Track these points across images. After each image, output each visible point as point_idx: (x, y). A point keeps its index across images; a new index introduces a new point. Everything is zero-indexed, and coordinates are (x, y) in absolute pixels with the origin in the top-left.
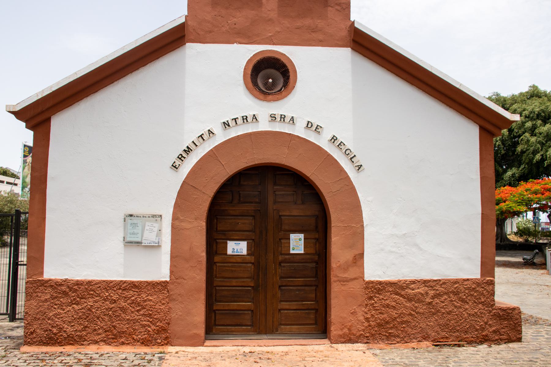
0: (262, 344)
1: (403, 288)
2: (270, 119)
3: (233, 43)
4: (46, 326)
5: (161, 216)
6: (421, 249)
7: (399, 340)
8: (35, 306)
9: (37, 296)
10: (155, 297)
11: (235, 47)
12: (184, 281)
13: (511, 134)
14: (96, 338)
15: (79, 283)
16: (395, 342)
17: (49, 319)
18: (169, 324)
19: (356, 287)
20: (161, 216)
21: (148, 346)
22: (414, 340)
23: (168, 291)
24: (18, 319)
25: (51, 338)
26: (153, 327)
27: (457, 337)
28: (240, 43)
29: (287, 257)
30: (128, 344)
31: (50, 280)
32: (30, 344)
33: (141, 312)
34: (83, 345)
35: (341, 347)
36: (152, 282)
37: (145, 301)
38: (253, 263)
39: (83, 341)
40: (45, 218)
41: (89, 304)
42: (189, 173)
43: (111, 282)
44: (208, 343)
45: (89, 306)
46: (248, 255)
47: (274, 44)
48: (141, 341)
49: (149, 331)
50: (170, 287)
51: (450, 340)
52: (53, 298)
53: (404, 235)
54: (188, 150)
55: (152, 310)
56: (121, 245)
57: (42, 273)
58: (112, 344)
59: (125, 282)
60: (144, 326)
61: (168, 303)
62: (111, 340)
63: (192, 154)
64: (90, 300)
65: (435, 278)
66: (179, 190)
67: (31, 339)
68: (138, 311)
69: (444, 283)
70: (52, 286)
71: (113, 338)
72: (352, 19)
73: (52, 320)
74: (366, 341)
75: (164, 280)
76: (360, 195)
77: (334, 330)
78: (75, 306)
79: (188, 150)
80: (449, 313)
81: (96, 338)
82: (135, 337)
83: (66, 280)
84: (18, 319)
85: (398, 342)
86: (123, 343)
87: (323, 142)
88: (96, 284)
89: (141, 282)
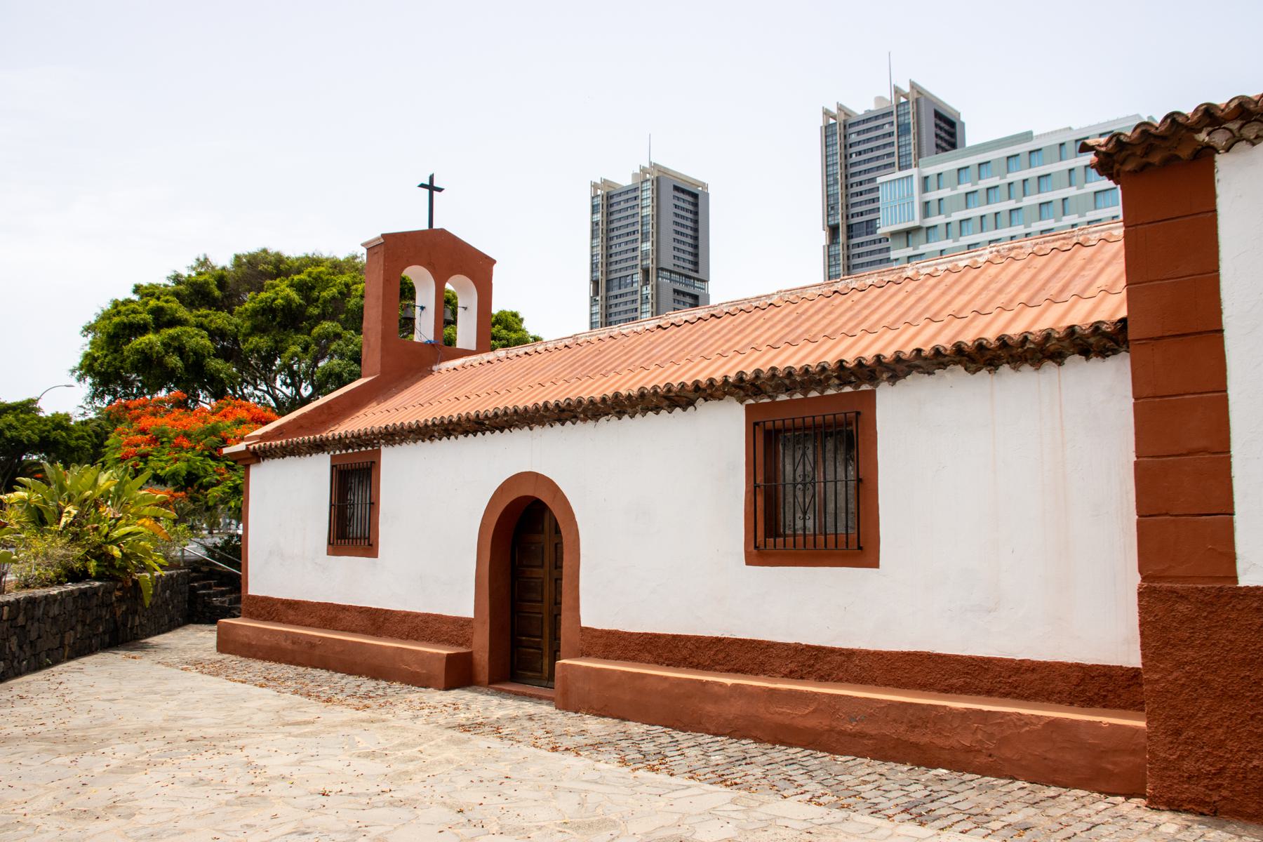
42: (502, 513)
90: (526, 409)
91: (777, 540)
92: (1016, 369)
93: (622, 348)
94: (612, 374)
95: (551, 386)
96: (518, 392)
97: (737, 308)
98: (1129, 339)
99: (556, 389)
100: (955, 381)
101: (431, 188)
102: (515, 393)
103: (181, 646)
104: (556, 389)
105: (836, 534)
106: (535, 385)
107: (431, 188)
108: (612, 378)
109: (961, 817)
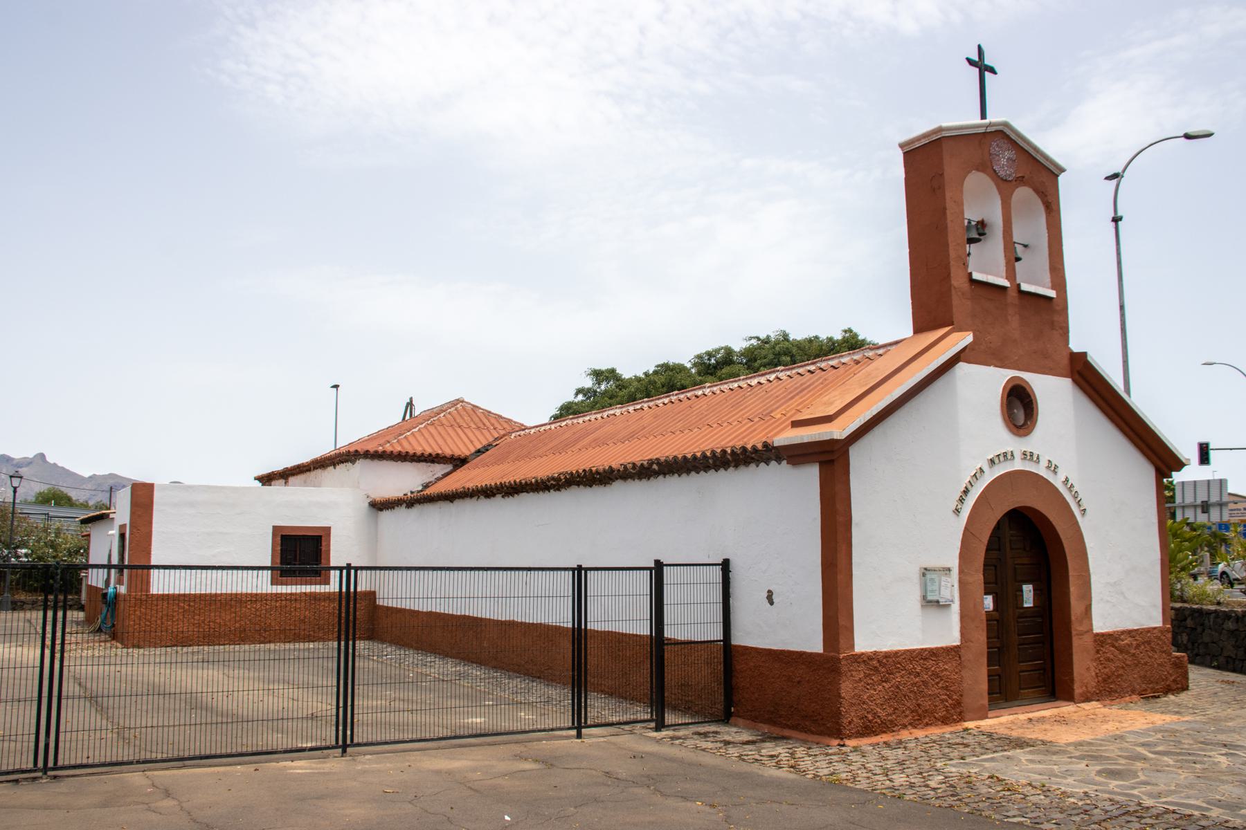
0: (1027, 711)
1: (1116, 640)
2: (1023, 457)
3: (990, 366)
4: (861, 713)
5: (925, 571)
6: (1125, 597)
7: (1117, 695)
8: (851, 688)
9: (852, 675)
10: (950, 665)
11: (992, 370)
12: (972, 644)
13: (753, 458)
14: (905, 721)
15: (887, 655)
16: (1115, 698)
17: (864, 703)
18: (961, 696)
19: (1088, 639)
20: (925, 571)
21: (947, 724)
22: (1127, 695)
23: (960, 657)
24: (668, 726)
25: (866, 727)
26: (950, 701)
27: (1152, 689)
28: (996, 366)
29: (1022, 611)
30: (931, 724)
31: (863, 654)
32: (849, 736)
33: (940, 685)
34: (894, 731)
35: (1082, 705)
36: (947, 647)
37: (942, 671)
38: (997, 620)
39: (894, 727)
40: (852, 575)
41: (897, 680)
42: (968, 517)
43: (914, 651)
44: (991, 714)
45: (897, 683)
46: (994, 610)
47: (1019, 370)
48: (941, 720)
49: (947, 707)
50: (962, 652)
51: (1148, 692)
52: (866, 676)
53: (1115, 583)
54: (966, 492)
55: (948, 682)
56: (918, 605)
57: (852, 646)
58: (918, 727)
59: (925, 650)
60: (943, 701)
61: (960, 671)
62: (917, 722)
63: (969, 495)
64: (898, 675)
65: (1135, 628)
66: (962, 539)
67: (849, 730)
68: (937, 683)
69: (1141, 633)
70: (864, 661)
71: (918, 720)
72: (1075, 345)
73: (867, 704)
74: (1097, 698)
75: (955, 644)
76: (1086, 541)
77: (1078, 690)
78: (884, 684)
79: (966, 492)
80: (1146, 664)
81: (905, 721)
82: (937, 716)
83: (875, 653)
84: (668, 726)
85: (1117, 698)
86: (927, 724)
87: (1057, 482)
88: (901, 655)
89: (937, 649)
90: (604, 470)
91: (1218, 499)
92: (706, 472)
93: (784, 389)
94: (627, 442)
95: (727, 426)
96: (689, 432)
97: (840, 362)
98: (158, 556)
99: (731, 429)
100: (402, 511)
101: (981, 66)
102: (735, 426)
103: (982, 737)
104: (683, 436)
105: (109, 688)
106: (676, 431)
107: (981, 66)
108: (652, 440)
109: (745, 758)
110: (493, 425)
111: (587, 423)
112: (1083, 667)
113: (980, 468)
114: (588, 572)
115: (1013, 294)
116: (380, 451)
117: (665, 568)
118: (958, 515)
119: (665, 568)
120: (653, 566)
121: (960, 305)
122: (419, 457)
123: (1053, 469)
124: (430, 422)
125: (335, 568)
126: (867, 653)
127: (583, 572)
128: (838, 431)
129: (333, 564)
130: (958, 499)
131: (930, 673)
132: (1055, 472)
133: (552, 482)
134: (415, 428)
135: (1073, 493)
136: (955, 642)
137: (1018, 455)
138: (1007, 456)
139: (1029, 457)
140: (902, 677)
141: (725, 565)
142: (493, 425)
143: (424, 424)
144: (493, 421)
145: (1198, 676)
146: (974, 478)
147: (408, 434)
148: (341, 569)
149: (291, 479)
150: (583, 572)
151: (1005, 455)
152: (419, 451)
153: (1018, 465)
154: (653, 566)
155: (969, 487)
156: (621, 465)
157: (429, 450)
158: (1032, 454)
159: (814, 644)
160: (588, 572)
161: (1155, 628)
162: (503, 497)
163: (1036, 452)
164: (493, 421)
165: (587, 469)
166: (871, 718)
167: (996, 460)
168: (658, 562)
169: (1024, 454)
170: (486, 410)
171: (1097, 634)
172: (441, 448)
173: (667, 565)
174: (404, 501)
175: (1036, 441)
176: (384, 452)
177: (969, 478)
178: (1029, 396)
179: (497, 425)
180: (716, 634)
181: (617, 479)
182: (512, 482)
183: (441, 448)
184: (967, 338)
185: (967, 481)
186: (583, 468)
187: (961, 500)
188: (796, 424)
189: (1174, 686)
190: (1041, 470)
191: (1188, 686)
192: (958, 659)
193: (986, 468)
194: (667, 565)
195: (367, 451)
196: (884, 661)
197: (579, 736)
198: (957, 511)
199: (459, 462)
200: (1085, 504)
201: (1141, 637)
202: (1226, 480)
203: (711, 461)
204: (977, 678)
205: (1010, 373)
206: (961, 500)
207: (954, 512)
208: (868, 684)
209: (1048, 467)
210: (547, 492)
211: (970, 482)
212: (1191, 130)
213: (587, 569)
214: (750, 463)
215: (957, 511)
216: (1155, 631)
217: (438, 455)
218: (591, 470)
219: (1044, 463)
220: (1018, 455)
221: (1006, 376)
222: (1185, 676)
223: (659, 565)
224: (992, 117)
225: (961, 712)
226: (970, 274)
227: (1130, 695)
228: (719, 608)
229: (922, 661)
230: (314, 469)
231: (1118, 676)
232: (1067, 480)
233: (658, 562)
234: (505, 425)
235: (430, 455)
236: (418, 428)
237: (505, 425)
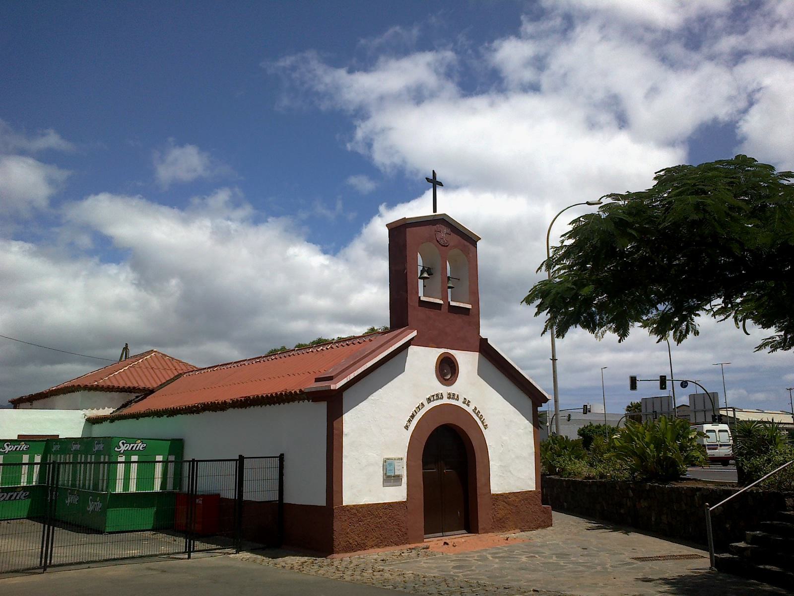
6: (512, 473)
15: (362, 506)
30: (388, 546)
36: (399, 502)
85: (506, 531)
87: (469, 410)
110: (174, 367)
111: (229, 368)
112: (484, 515)
113: (422, 403)
114: (199, 463)
115: (445, 309)
116: (95, 385)
117: (245, 459)
118: (407, 430)
119: (245, 459)
120: (238, 458)
121: (414, 313)
122: (121, 389)
123: (467, 403)
124: (131, 365)
125: (187, 461)
126: (350, 505)
127: (195, 463)
128: (336, 386)
129: (185, 459)
130: (407, 420)
131: (388, 517)
132: (468, 405)
133: (194, 409)
134: (121, 369)
135: (479, 416)
136: (404, 499)
137: (445, 396)
138: (439, 397)
139: (452, 396)
140: (371, 519)
141: (281, 458)
142: (174, 367)
143: (127, 367)
144: (175, 364)
145: (558, 517)
146: (418, 409)
147: (116, 373)
148: (189, 461)
149: (35, 403)
150: (195, 463)
151: (437, 395)
152: (122, 385)
153: (445, 401)
154: (238, 458)
155: (415, 414)
156: (231, 400)
157: (129, 384)
158: (454, 395)
159: (322, 502)
160: (199, 463)
161: (531, 491)
162: (167, 417)
163: (456, 393)
164: (175, 364)
165: (213, 402)
166: (351, 542)
167: (432, 399)
168: (240, 456)
169: (449, 394)
170: (171, 358)
171: (493, 495)
172: (137, 383)
173: (246, 458)
174: (108, 419)
175: (457, 388)
176: (97, 386)
177: (414, 409)
178: (453, 363)
179: (177, 367)
180: (275, 497)
181: (229, 408)
182: (172, 408)
183: (137, 383)
184: (415, 333)
185: (414, 410)
186: (211, 401)
187: (410, 421)
188: (318, 380)
189: (543, 524)
190: (459, 403)
191: (552, 524)
192: (406, 508)
193: (425, 403)
194: (246, 458)
195: (86, 385)
196: (361, 510)
197: (189, 557)
198: (407, 427)
199: (148, 392)
200: (486, 423)
201: (524, 496)
202: (717, 393)
203: (275, 399)
204: (419, 520)
205: (439, 352)
206: (410, 421)
207: (405, 427)
208: (350, 523)
209: (464, 403)
210: (192, 414)
211: (415, 411)
212: (590, 201)
213: (198, 461)
214: (295, 400)
215: (407, 427)
216: (530, 493)
217: (134, 388)
218: (215, 402)
219: (461, 399)
220: (445, 396)
221: (439, 353)
222: (550, 518)
223: (241, 459)
224: (438, 212)
225: (407, 539)
226: (420, 297)
227: (514, 529)
228: (277, 482)
229: (383, 510)
230: (50, 396)
231: (507, 518)
232: (476, 408)
233: (240, 456)
234: (183, 367)
235: (129, 387)
236: (123, 370)
237: (183, 367)
